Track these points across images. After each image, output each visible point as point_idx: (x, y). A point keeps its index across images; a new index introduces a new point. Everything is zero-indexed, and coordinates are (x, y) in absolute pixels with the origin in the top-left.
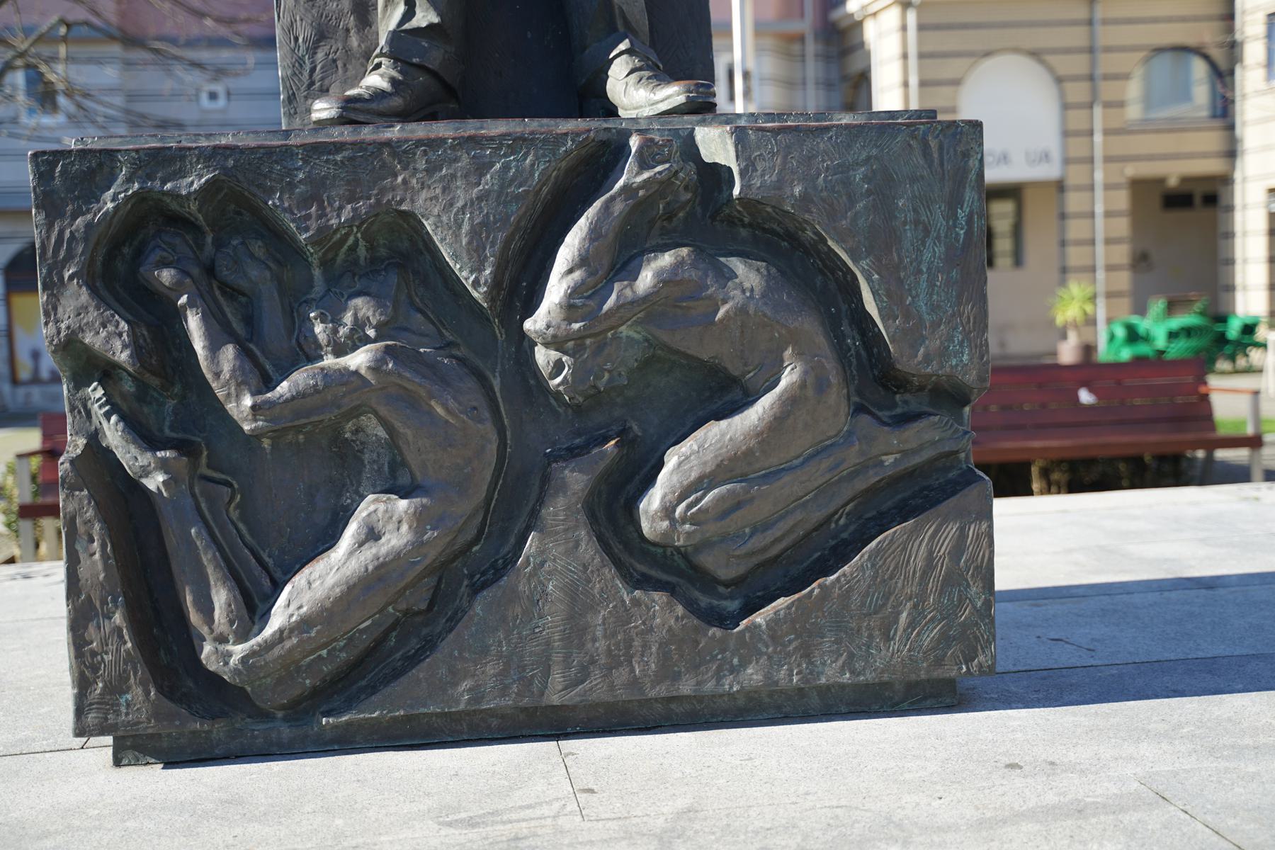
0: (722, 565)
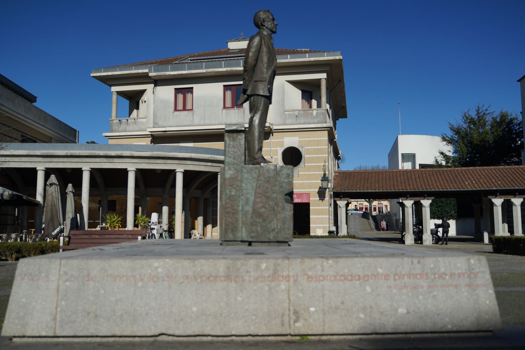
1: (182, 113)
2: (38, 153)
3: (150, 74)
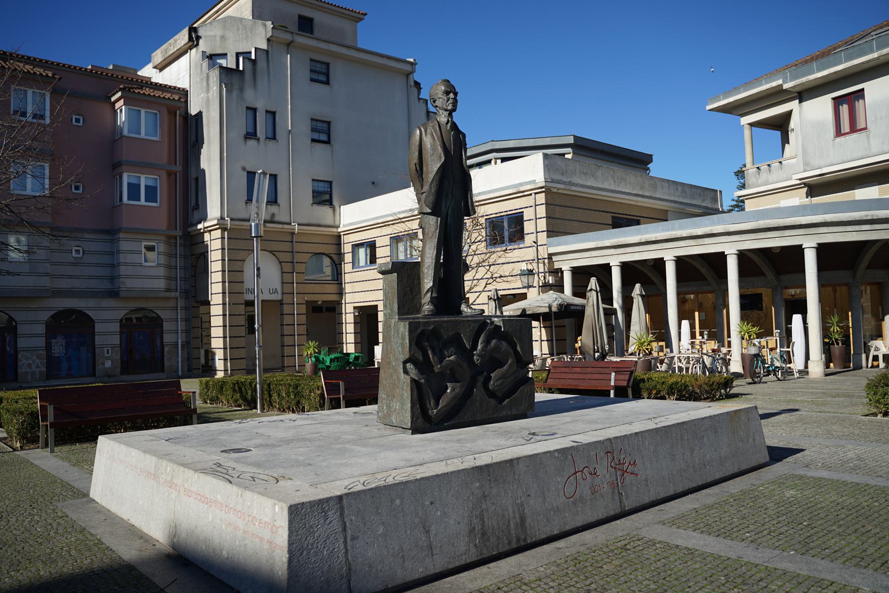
0: (499, 394)
1: (848, 137)
2: (607, 243)
3: (785, 86)
